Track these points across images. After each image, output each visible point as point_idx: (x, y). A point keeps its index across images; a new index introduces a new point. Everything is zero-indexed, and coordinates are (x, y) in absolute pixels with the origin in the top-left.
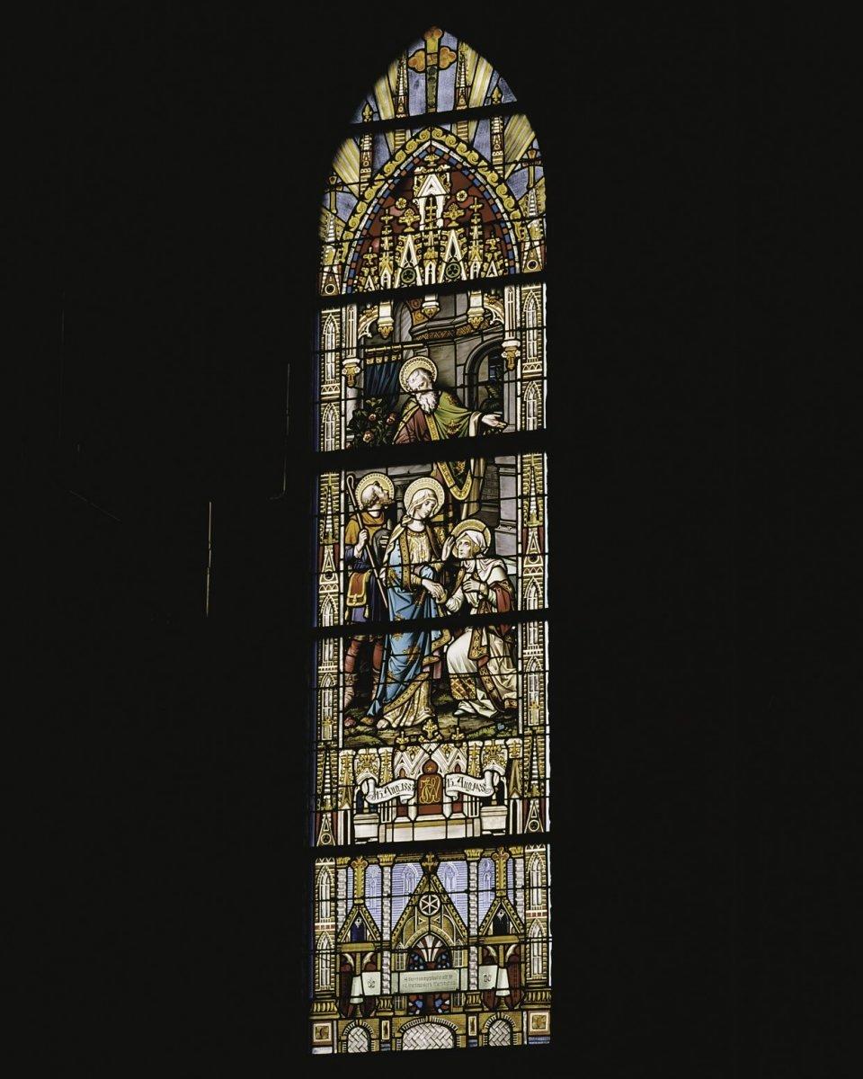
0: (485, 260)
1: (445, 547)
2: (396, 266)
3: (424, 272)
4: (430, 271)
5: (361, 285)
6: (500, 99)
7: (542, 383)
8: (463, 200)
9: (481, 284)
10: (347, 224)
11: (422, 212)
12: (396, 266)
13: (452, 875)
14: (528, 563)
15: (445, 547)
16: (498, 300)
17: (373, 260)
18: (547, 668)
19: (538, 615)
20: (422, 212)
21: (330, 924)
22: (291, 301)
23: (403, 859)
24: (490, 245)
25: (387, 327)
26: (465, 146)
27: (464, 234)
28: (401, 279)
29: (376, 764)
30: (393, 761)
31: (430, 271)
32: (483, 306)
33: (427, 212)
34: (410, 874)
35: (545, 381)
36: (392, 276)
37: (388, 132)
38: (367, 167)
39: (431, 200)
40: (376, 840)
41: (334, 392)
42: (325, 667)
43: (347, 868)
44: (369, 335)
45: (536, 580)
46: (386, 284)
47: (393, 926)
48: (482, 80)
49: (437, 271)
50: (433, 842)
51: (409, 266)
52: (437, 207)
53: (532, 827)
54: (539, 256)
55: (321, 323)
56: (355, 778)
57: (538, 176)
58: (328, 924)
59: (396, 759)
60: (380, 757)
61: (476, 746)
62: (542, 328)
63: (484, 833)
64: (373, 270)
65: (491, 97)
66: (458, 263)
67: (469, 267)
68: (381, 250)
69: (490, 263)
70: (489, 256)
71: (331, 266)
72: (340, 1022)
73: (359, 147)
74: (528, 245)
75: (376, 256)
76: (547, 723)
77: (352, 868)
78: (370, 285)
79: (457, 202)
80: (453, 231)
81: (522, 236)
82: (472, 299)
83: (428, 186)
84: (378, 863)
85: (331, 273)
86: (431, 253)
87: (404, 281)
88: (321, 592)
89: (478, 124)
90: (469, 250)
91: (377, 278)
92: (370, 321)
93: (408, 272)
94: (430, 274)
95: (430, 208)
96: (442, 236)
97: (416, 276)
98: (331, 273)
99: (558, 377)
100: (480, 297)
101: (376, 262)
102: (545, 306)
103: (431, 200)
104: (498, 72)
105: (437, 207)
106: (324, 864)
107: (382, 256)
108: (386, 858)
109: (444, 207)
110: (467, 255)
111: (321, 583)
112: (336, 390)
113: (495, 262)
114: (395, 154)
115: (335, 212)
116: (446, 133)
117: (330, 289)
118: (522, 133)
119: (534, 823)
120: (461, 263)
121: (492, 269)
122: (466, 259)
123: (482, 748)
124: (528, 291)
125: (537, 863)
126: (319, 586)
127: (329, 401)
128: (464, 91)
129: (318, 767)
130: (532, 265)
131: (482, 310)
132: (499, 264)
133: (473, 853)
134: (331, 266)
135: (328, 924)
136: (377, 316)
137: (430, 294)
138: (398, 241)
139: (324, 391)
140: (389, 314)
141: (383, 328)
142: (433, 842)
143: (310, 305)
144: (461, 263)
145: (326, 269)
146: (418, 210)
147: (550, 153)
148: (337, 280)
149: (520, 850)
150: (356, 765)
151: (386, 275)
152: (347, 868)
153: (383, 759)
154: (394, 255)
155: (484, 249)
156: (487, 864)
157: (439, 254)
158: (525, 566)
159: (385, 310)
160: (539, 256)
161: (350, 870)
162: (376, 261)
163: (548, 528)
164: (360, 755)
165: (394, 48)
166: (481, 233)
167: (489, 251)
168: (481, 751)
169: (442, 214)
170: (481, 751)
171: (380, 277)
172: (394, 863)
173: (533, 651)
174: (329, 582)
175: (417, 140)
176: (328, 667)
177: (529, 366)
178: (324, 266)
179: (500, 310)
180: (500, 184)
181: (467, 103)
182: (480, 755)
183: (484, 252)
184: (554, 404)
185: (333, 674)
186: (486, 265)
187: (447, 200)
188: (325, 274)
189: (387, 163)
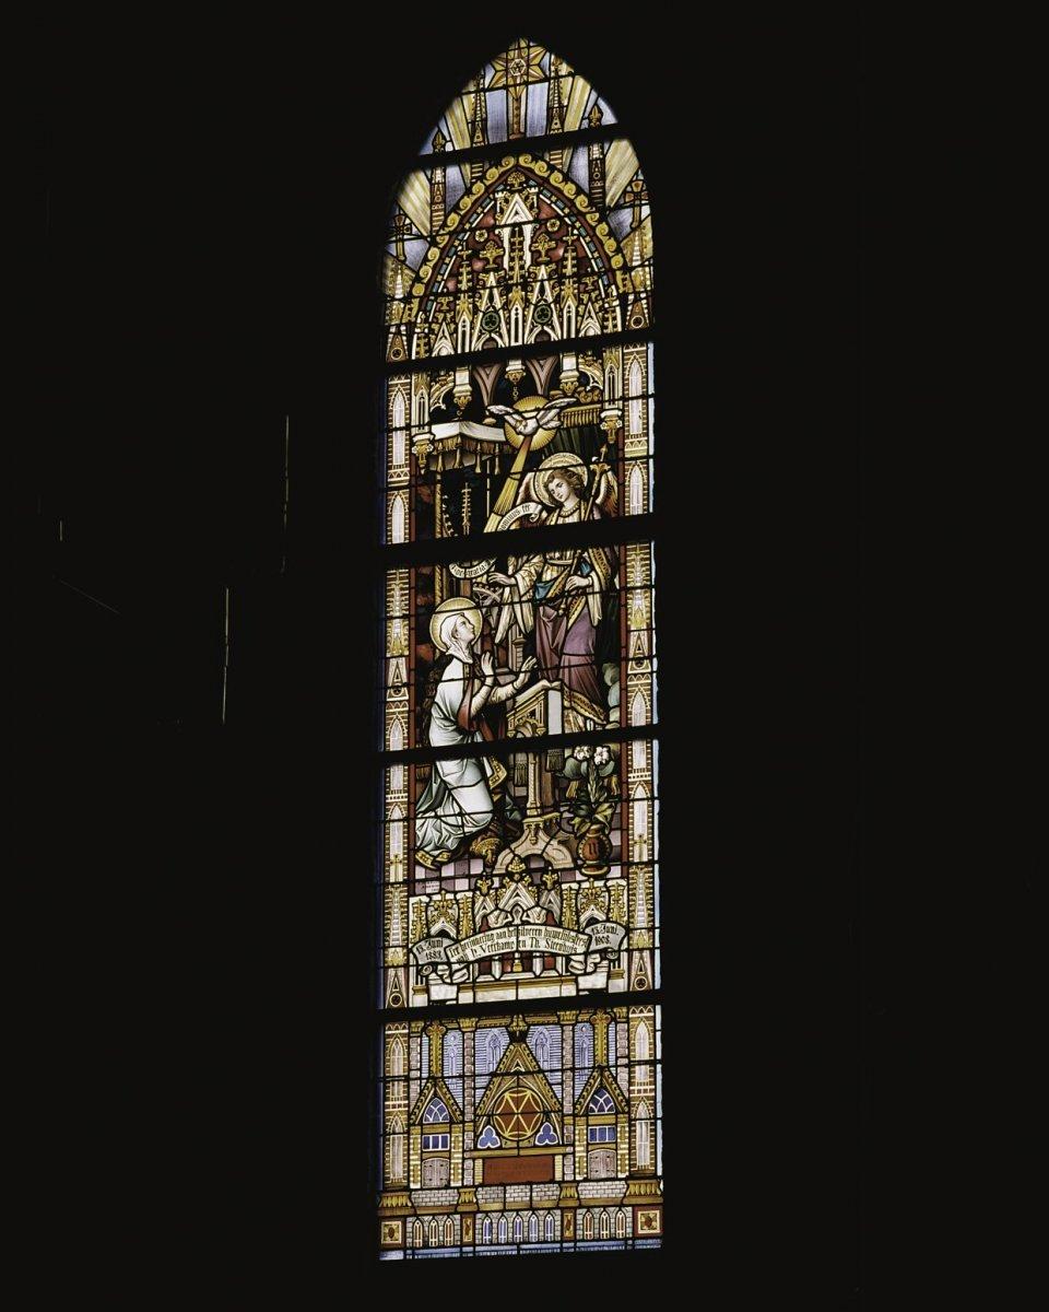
0: (580, 302)
2: (476, 310)
3: (509, 317)
4: (517, 314)
5: (433, 333)
6: (599, 120)
7: (647, 463)
8: (556, 229)
9: (579, 345)
10: (417, 273)
11: (506, 245)
12: (476, 310)
13: (545, 1039)
14: (632, 669)
16: (596, 361)
17: (448, 303)
18: (659, 1115)
19: (645, 733)
20: (506, 245)
21: (403, 1102)
22: (354, 363)
23: (488, 1022)
24: (586, 284)
25: (465, 397)
26: (561, 176)
27: (555, 271)
28: (481, 325)
29: (453, 912)
30: (473, 911)
31: (517, 314)
32: (577, 369)
33: (512, 244)
34: (492, 1043)
35: (651, 461)
36: (472, 322)
37: (464, 163)
39: (517, 229)
40: (454, 1002)
41: (402, 478)
44: (443, 407)
46: (441, 571)
48: (580, 94)
49: (524, 316)
50: (523, 1014)
51: (491, 309)
52: (522, 266)
53: (638, 985)
55: (388, 392)
56: (429, 929)
57: (643, 216)
58: (646, 1087)
59: (477, 906)
60: (458, 903)
61: (571, 889)
62: (648, 457)
63: (581, 993)
64: (449, 316)
65: (588, 118)
66: (549, 306)
67: (562, 310)
68: (458, 291)
69: (586, 305)
70: (585, 297)
71: (398, 326)
73: (430, 180)
74: (631, 297)
75: (451, 299)
76: (657, 925)
77: (429, 1036)
78: (444, 348)
79: (548, 233)
80: (543, 266)
83: (514, 212)
84: (460, 1029)
85: (398, 333)
86: (517, 294)
87: (486, 328)
90: (561, 290)
91: (453, 326)
92: (445, 389)
93: (491, 317)
94: (519, 331)
95: (517, 240)
96: (530, 273)
97: (500, 321)
98: (398, 333)
99: (665, 459)
100: (574, 360)
101: (452, 307)
102: (651, 493)
103: (517, 229)
104: (596, 91)
105: (522, 266)
106: (396, 1031)
107: (459, 298)
108: (466, 1023)
109: (532, 238)
110: (559, 295)
113: (592, 304)
114: (471, 187)
115: (402, 258)
116: (535, 159)
117: (397, 353)
118: (622, 160)
119: (641, 980)
120: (552, 306)
121: (589, 312)
122: (558, 300)
123: (578, 891)
124: (632, 353)
125: (644, 1034)
127: (398, 488)
128: (556, 111)
131: (576, 373)
132: (597, 306)
133: (568, 1015)
134: (398, 326)
135: (646, 1087)
136: (451, 384)
137: (515, 358)
138: (479, 280)
139: (391, 477)
140: (467, 381)
141: (459, 398)
142: (523, 1014)
143: (368, 372)
144: (552, 306)
145: (393, 330)
146: (502, 242)
147: (656, 178)
148: (646, 311)
150: (429, 913)
151: (464, 321)
152: (421, 1037)
153: (461, 906)
154: (473, 297)
155: (578, 288)
156: (584, 1031)
157: (526, 295)
158: (629, 672)
159: (462, 377)
161: (425, 1039)
162: (452, 305)
163: (655, 474)
164: (435, 902)
166: (575, 270)
167: (586, 292)
168: (577, 894)
169: (530, 246)
170: (577, 894)
171: (457, 325)
172: (477, 1028)
173: (640, 774)
178: (390, 326)
179: (598, 374)
180: (552, 172)
181: (562, 123)
182: (576, 899)
183: (579, 293)
184: (685, 1179)
185: (402, 803)
186: (581, 309)
187: (535, 231)
188: (391, 336)
189: (462, 197)
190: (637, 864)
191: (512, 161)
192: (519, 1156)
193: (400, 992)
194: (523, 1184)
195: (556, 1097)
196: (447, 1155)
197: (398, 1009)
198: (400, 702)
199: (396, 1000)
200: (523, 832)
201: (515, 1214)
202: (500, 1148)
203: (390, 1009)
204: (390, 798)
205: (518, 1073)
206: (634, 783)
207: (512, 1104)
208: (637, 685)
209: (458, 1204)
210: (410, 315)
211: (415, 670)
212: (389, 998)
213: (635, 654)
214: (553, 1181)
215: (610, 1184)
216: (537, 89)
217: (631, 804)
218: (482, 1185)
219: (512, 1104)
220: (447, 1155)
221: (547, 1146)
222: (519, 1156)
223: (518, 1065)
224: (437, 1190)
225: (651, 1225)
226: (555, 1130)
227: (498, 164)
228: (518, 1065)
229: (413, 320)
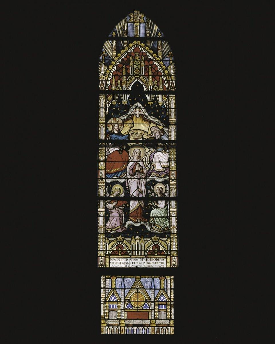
1: (141, 157)
14: (171, 181)
15: (141, 157)
38: (115, 51)
42: (101, 209)
43: (109, 279)
45: (174, 187)
47: (125, 296)
50: (136, 283)
52: (134, 54)
53: (101, 266)
54: (175, 86)
57: (133, 109)
72: (154, 67)
81: (169, 78)
82: (103, 109)
85: (102, 83)
88: (99, 185)
89: (118, 216)
105: (134, 54)
111: (99, 182)
112: (104, 121)
126: (98, 182)
129: (98, 241)
130: (172, 88)
142: (136, 283)
149: (169, 277)
160: (175, 86)
165: (123, 15)
174: (102, 182)
175: (132, 44)
176: (101, 209)
177: (172, 120)
184: (179, 321)
190: (173, 234)
191: (136, 42)
192: (138, 311)
193: (103, 263)
194: (131, 319)
195: (149, 296)
196: (165, 310)
197: (175, 267)
198: (174, 183)
199: (101, 265)
200: (108, 222)
201: (117, 327)
202: (133, 309)
203: (100, 267)
204: (99, 210)
205: (138, 289)
206: (100, 212)
207: (134, 298)
208: (172, 186)
209: (120, 324)
210: (106, 78)
211: (100, 161)
212: (100, 265)
213: (101, 177)
214: (148, 319)
215: (163, 320)
216: (138, 25)
217: (171, 217)
218: (127, 319)
219: (134, 298)
220: (165, 310)
221: (146, 309)
222: (138, 311)
223: (138, 286)
224: (113, 319)
225: (171, 331)
226: (149, 305)
227: (132, 43)
228: (138, 286)
229: (107, 79)
